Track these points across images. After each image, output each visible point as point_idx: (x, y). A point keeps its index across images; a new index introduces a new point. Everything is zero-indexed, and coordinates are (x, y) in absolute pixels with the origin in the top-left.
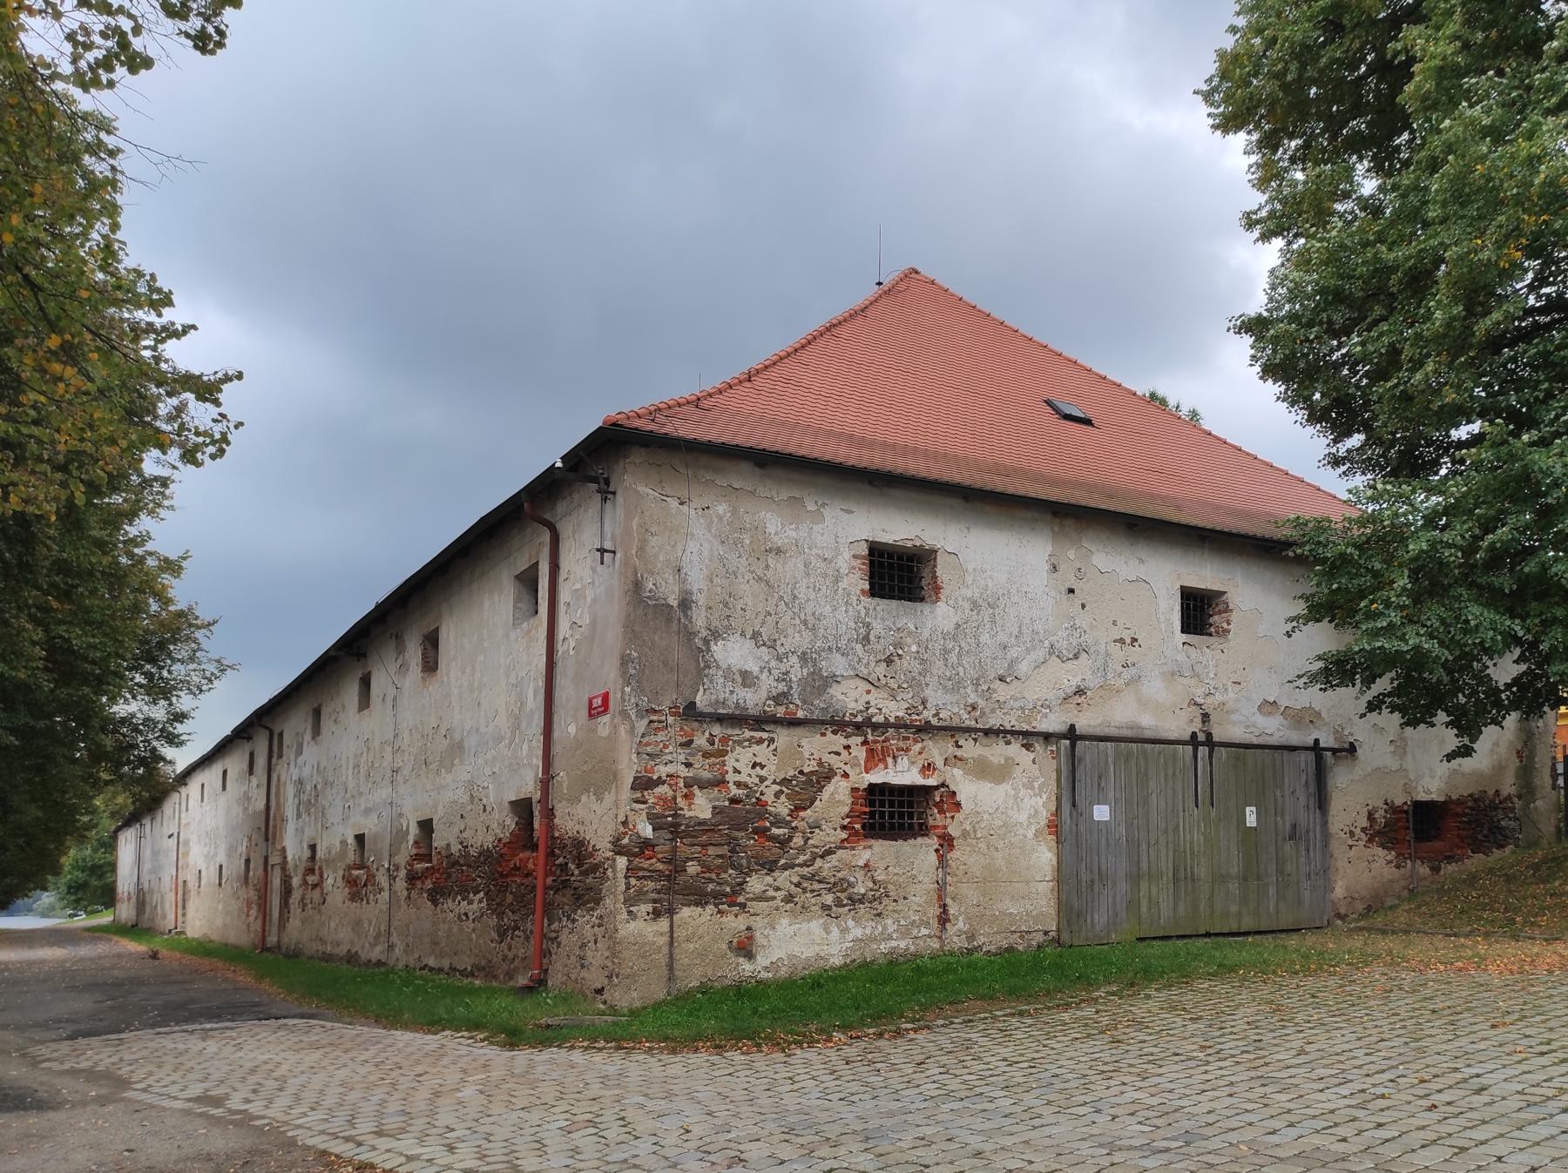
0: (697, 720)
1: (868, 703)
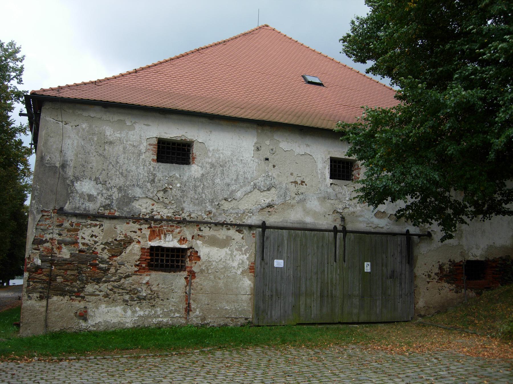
0: (65, 216)
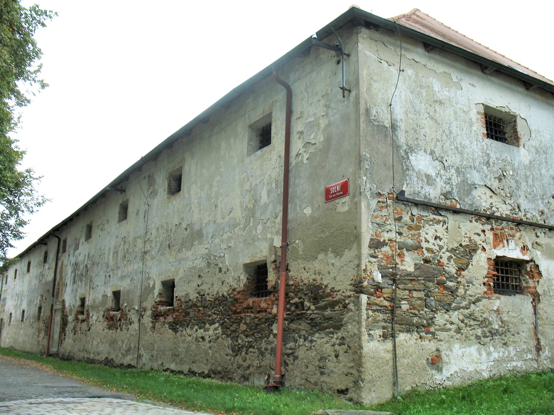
0: (404, 204)
1: (492, 204)
